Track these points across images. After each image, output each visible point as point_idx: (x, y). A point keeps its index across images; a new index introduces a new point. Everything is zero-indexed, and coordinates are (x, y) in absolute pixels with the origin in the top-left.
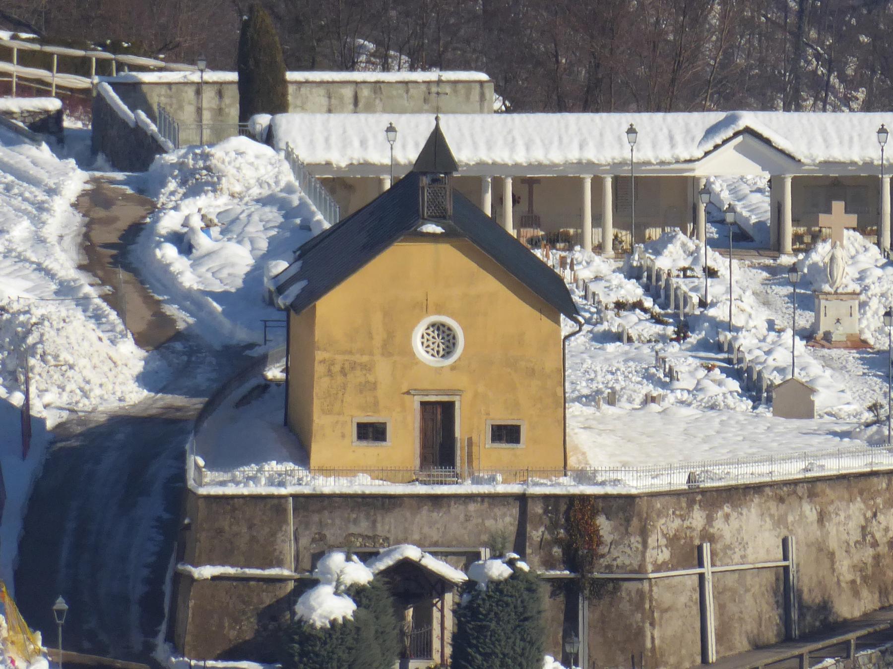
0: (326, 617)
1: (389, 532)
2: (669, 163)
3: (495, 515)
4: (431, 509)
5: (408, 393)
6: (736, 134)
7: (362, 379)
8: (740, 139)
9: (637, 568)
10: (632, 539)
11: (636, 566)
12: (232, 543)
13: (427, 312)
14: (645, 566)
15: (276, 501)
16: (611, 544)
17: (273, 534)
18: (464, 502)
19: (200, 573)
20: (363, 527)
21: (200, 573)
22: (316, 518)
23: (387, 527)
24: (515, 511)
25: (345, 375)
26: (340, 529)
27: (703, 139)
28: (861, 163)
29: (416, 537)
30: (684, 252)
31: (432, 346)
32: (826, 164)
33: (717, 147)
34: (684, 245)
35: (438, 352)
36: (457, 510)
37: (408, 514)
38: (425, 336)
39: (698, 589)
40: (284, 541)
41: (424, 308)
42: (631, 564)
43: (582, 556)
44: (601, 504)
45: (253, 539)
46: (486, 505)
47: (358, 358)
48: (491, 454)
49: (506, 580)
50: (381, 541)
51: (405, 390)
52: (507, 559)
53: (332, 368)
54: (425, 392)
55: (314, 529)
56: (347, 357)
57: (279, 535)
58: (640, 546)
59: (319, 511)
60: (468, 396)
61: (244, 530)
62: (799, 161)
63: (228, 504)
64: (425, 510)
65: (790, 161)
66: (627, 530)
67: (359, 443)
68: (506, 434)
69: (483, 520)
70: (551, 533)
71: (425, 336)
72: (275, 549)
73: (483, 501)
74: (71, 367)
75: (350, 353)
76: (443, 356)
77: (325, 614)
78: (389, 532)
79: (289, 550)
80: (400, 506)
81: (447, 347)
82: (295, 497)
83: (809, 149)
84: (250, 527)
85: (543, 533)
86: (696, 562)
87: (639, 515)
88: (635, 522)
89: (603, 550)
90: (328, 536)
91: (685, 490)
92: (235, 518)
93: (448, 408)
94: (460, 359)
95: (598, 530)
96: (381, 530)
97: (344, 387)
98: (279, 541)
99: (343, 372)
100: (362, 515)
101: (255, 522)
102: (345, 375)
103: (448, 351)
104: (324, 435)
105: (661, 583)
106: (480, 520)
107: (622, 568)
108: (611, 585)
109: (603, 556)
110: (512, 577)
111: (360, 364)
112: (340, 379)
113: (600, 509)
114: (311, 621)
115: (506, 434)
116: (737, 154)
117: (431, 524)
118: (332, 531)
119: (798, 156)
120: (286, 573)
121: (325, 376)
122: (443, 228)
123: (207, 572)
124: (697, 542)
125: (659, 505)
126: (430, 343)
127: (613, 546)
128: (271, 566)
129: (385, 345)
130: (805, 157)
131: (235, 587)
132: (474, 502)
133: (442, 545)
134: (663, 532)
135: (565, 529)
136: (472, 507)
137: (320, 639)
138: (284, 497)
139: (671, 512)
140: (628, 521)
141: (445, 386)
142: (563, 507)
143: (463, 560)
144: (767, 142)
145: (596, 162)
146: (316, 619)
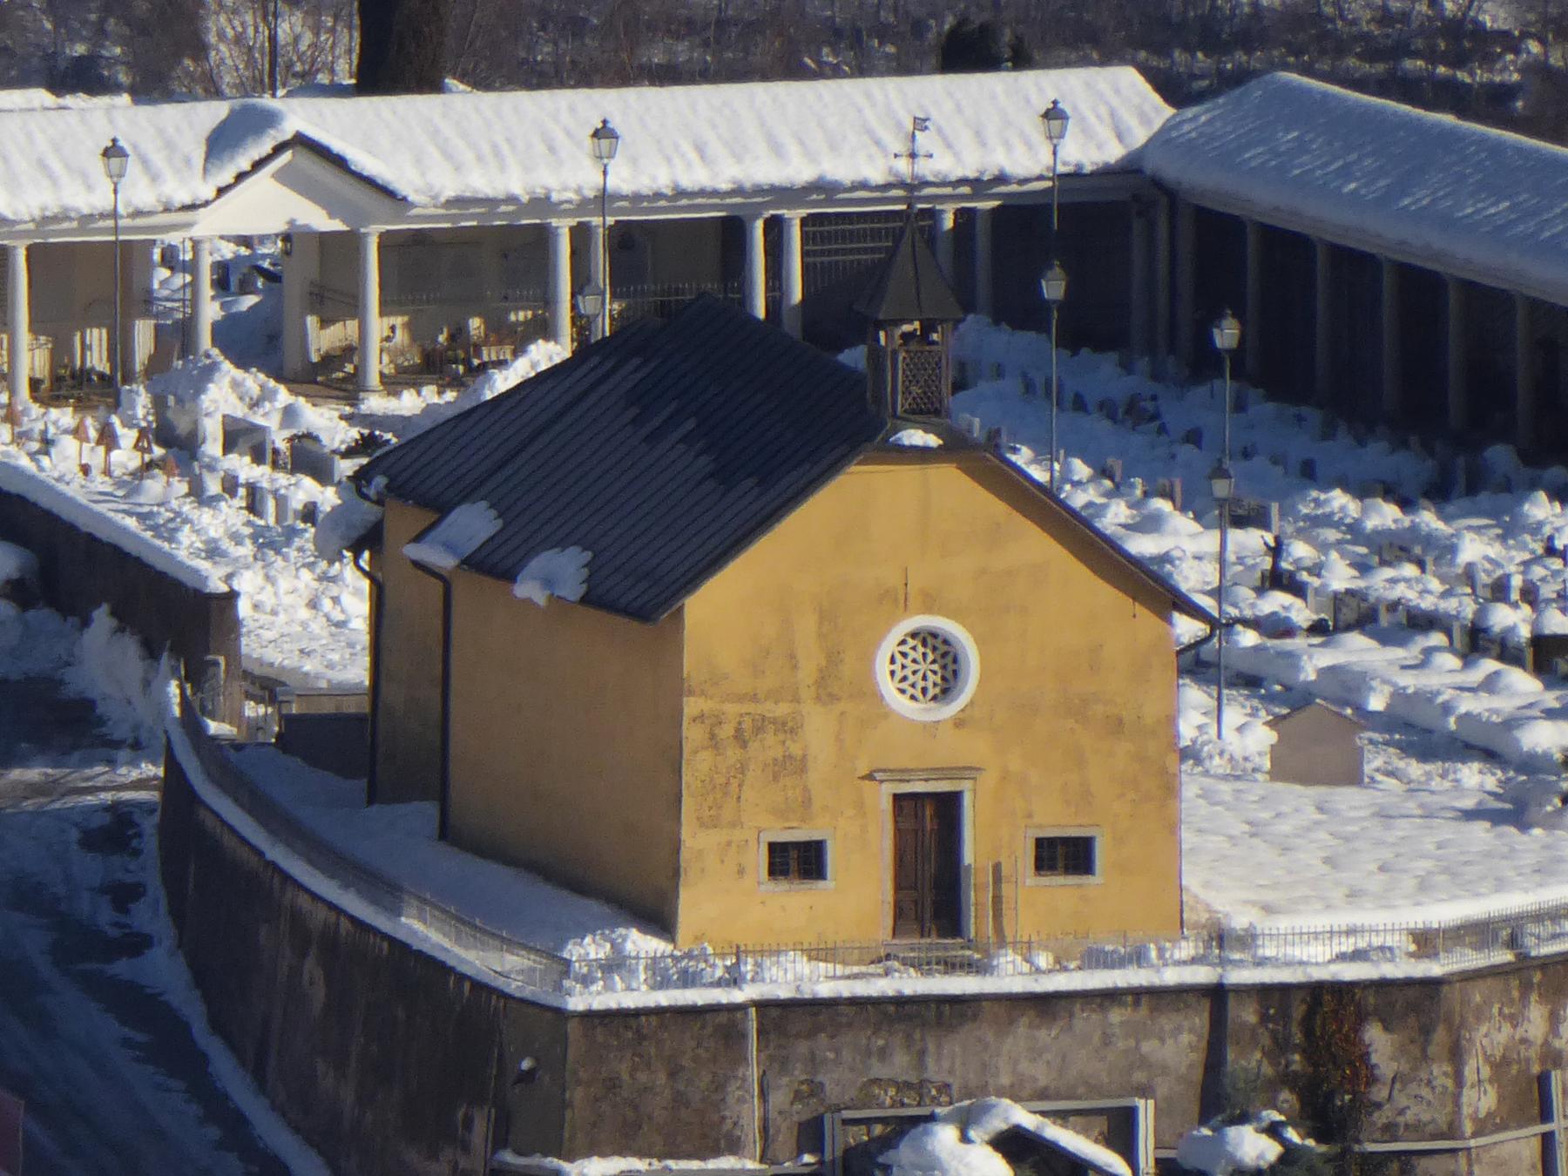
1: (951, 1072)
2: (150, 213)
3: (1162, 1029)
4: (1037, 1021)
5: (870, 777)
6: (279, 149)
8: (286, 157)
9: (1445, 1128)
10: (1436, 1071)
11: (1442, 1121)
12: (636, 1108)
13: (906, 609)
14: (1460, 1126)
15: (723, 1018)
17: (719, 1086)
20: (899, 1064)
22: (802, 1047)
23: (946, 1064)
24: (1200, 1020)
25: (744, 745)
26: (852, 1069)
27: (206, 160)
28: (525, 199)
29: (1005, 1080)
30: (241, 399)
31: (908, 672)
32: (458, 202)
33: (241, 177)
34: (236, 385)
35: (924, 691)
36: (1085, 1020)
37: (990, 1037)
38: (898, 657)
39: (1539, 1166)
40: (741, 1100)
41: (897, 601)
42: (1433, 1121)
43: (1342, 1108)
44: (1371, 1000)
45: (679, 1100)
46: (1144, 1011)
48: (1040, 899)
49: (1272, 1167)
50: (934, 1092)
51: (864, 772)
52: (1265, 1124)
54: (903, 774)
55: (799, 1073)
58: (1450, 1083)
59: (812, 1034)
60: (989, 779)
61: (662, 1078)
62: (404, 199)
64: (1022, 1027)
65: (387, 201)
66: (1424, 1050)
67: (772, 886)
68: (1066, 855)
70: (1274, 1063)
71: (898, 657)
72: (723, 1118)
73: (1137, 1003)
75: (754, 698)
76: (934, 698)
78: (951, 1072)
80: (975, 1017)
81: (944, 678)
82: (763, 1006)
83: (423, 174)
84: (672, 1075)
85: (1260, 1062)
86: (1536, 1110)
87: (1448, 1021)
88: (1440, 1036)
89: (1379, 1093)
90: (828, 1087)
91: (1509, 963)
92: (641, 1056)
93: (948, 806)
94: (972, 703)
95: (1368, 1054)
96: (935, 1071)
97: (743, 769)
98: (731, 1100)
100: (898, 1040)
102: (744, 745)
103: (947, 688)
104: (703, 870)
105: (1485, 1157)
106: (1132, 1043)
107: (1416, 1130)
108: (1395, 1166)
109: (1379, 1106)
110: (1282, 1159)
111: (774, 721)
112: (733, 754)
113: (1370, 1008)
115: (1066, 855)
116: (278, 186)
117: (1036, 1053)
118: (835, 1076)
119: (402, 187)
121: (704, 748)
122: (939, 435)
124: (1536, 1069)
125: (1478, 998)
127: (1398, 1086)
128: (716, 1152)
129: (822, 680)
130: (416, 191)
133: (1058, 1096)
134: (1485, 1053)
135: (1304, 1052)
136: (1116, 1016)
139: (1495, 1010)
140: (1426, 1031)
141: (941, 759)
142: (1298, 1011)
143: (1101, 1124)
144: (339, 162)
145: (11, 216)
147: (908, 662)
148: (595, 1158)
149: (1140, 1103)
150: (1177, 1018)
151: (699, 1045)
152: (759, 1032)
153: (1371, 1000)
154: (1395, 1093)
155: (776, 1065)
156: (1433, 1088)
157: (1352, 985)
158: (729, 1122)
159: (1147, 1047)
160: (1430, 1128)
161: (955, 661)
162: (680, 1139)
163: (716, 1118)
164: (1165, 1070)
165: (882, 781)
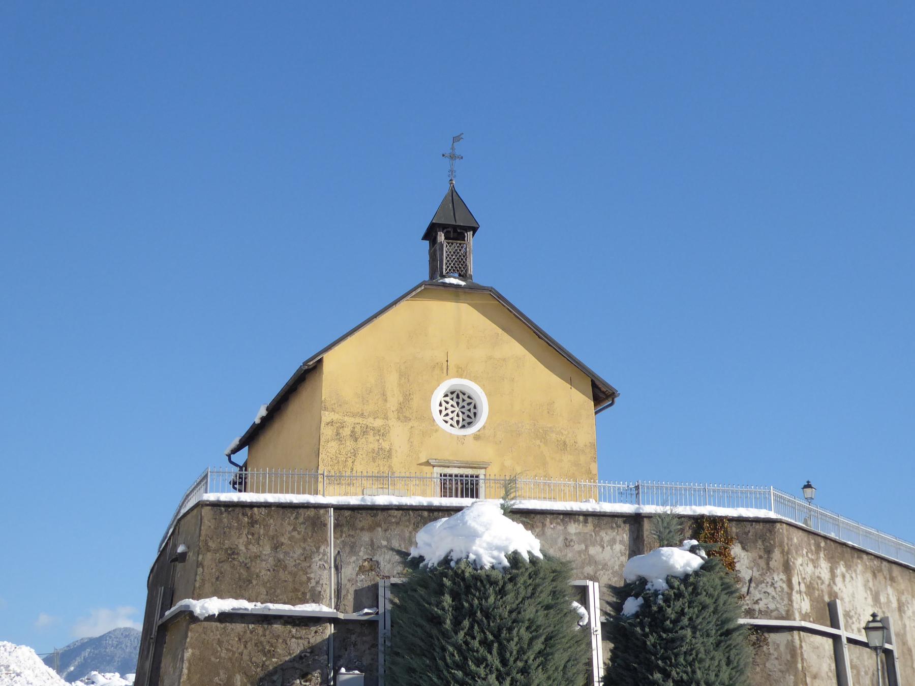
0: (499, 548)
3: (602, 540)
5: (427, 463)
7: (376, 446)
16: (750, 581)
17: (307, 558)
18: (562, 520)
19: (203, 607)
21: (203, 607)
22: (366, 537)
31: (467, 407)
35: (458, 422)
38: (470, 401)
41: (445, 370)
42: (777, 609)
44: (734, 529)
45: (279, 564)
46: (590, 527)
47: (370, 421)
49: (696, 573)
53: (341, 431)
56: (360, 420)
57: (316, 558)
59: (371, 529)
61: (267, 550)
63: (244, 515)
66: (768, 564)
69: (587, 547)
71: (470, 401)
72: (309, 579)
73: (586, 522)
74: (18, 675)
77: (497, 542)
79: (328, 581)
84: (276, 547)
88: (777, 555)
92: (253, 534)
94: (484, 427)
98: (315, 567)
99: (354, 437)
101: (283, 540)
106: (583, 547)
111: (373, 429)
112: (350, 444)
113: (734, 535)
114: (472, 557)
120: (324, 609)
123: (214, 605)
126: (465, 404)
127: (753, 585)
128: (303, 601)
129: (400, 410)
131: (251, 632)
132: (575, 521)
136: (573, 528)
137: (493, 583)
138: (326, 507)
140: (769, 551)
146: (481, 551)
147: (449, 406)
148: (215, 598)
149: (590, 584)
150: (612, 534)
151: (295, 529)
152: (336, 526)
153: (734, 529)
154: (751, 589)
155: (347, 549)
156: (775, 588)
157: (721, 519)
158: (313, 581)
159: (592, 551)
160: (774, 614)
161: (475, 407)
162: (279, 591)
163: (304, 578)
164: (605, 566)
165: (434, 466)
